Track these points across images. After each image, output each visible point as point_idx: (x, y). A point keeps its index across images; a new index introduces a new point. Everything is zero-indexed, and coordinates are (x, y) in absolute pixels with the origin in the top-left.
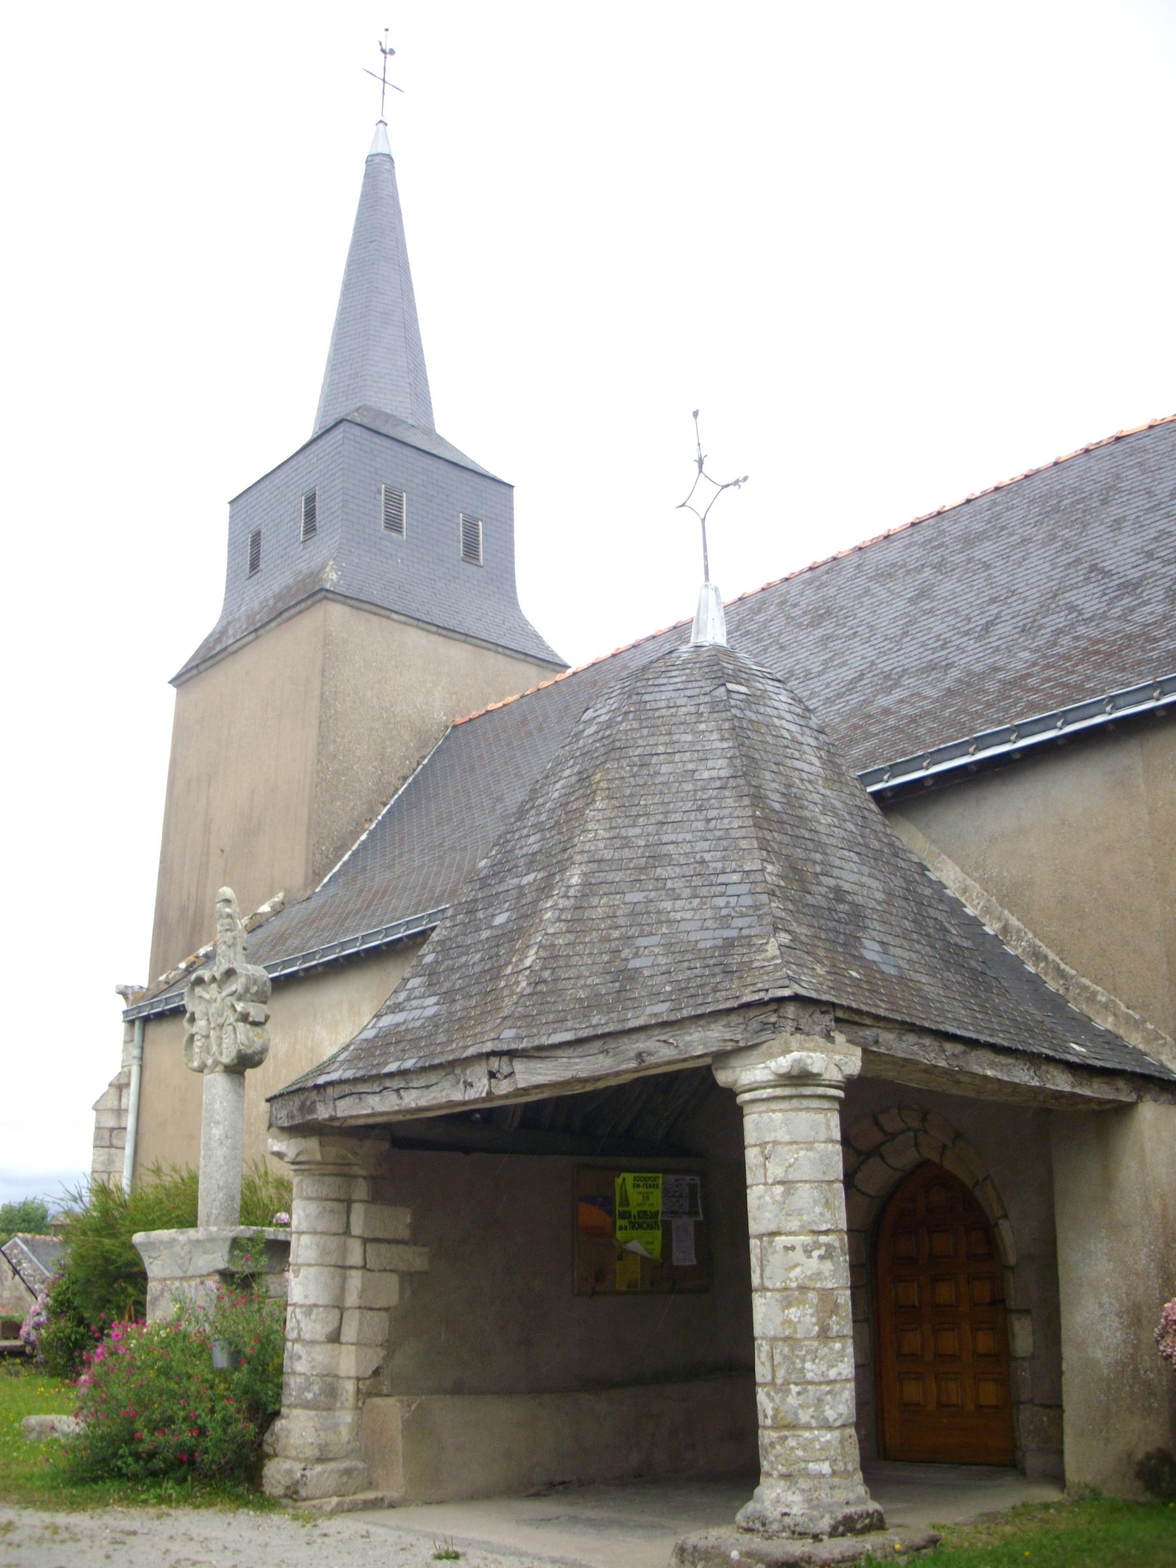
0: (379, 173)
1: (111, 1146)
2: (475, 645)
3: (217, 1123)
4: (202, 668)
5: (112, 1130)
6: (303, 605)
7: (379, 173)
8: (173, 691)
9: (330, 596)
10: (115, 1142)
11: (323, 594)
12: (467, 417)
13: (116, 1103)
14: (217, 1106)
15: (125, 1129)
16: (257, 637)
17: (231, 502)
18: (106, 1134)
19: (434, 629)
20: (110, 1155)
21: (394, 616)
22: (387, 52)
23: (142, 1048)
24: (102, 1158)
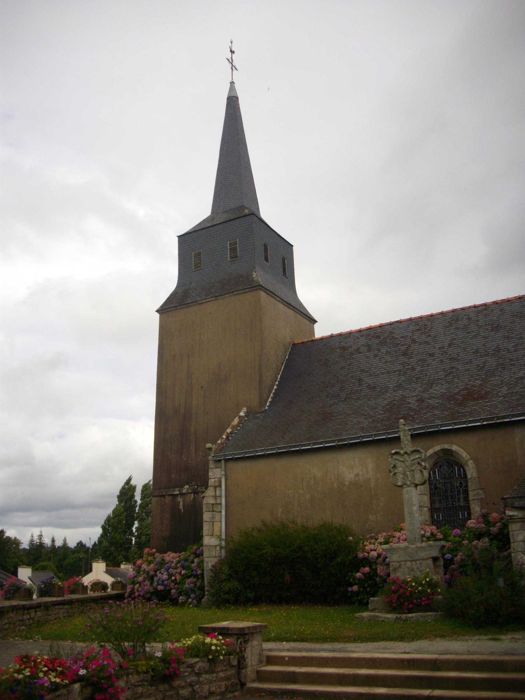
0: (232, 103)
1: (213, 511)
2: (295, 312)
3: (414, 505)
4: (178, 308)
5: (213, 504)
6: (247, 290)
7: (232, 103)
8: (158, 315)
9: (262, 288)
10: (215, 509)
11: (260, 287)
12: (272, 210)
13: (214, 493)
14: (414, 499)
15: (221, 504)
16: (216, 299)
17: (179, 237)
18: (211, 507)
19: (286, 304)
20: (213, 514)
21: (277, 298)
22: (232, 52)
23: (225, 471)
24: (209, 516)
